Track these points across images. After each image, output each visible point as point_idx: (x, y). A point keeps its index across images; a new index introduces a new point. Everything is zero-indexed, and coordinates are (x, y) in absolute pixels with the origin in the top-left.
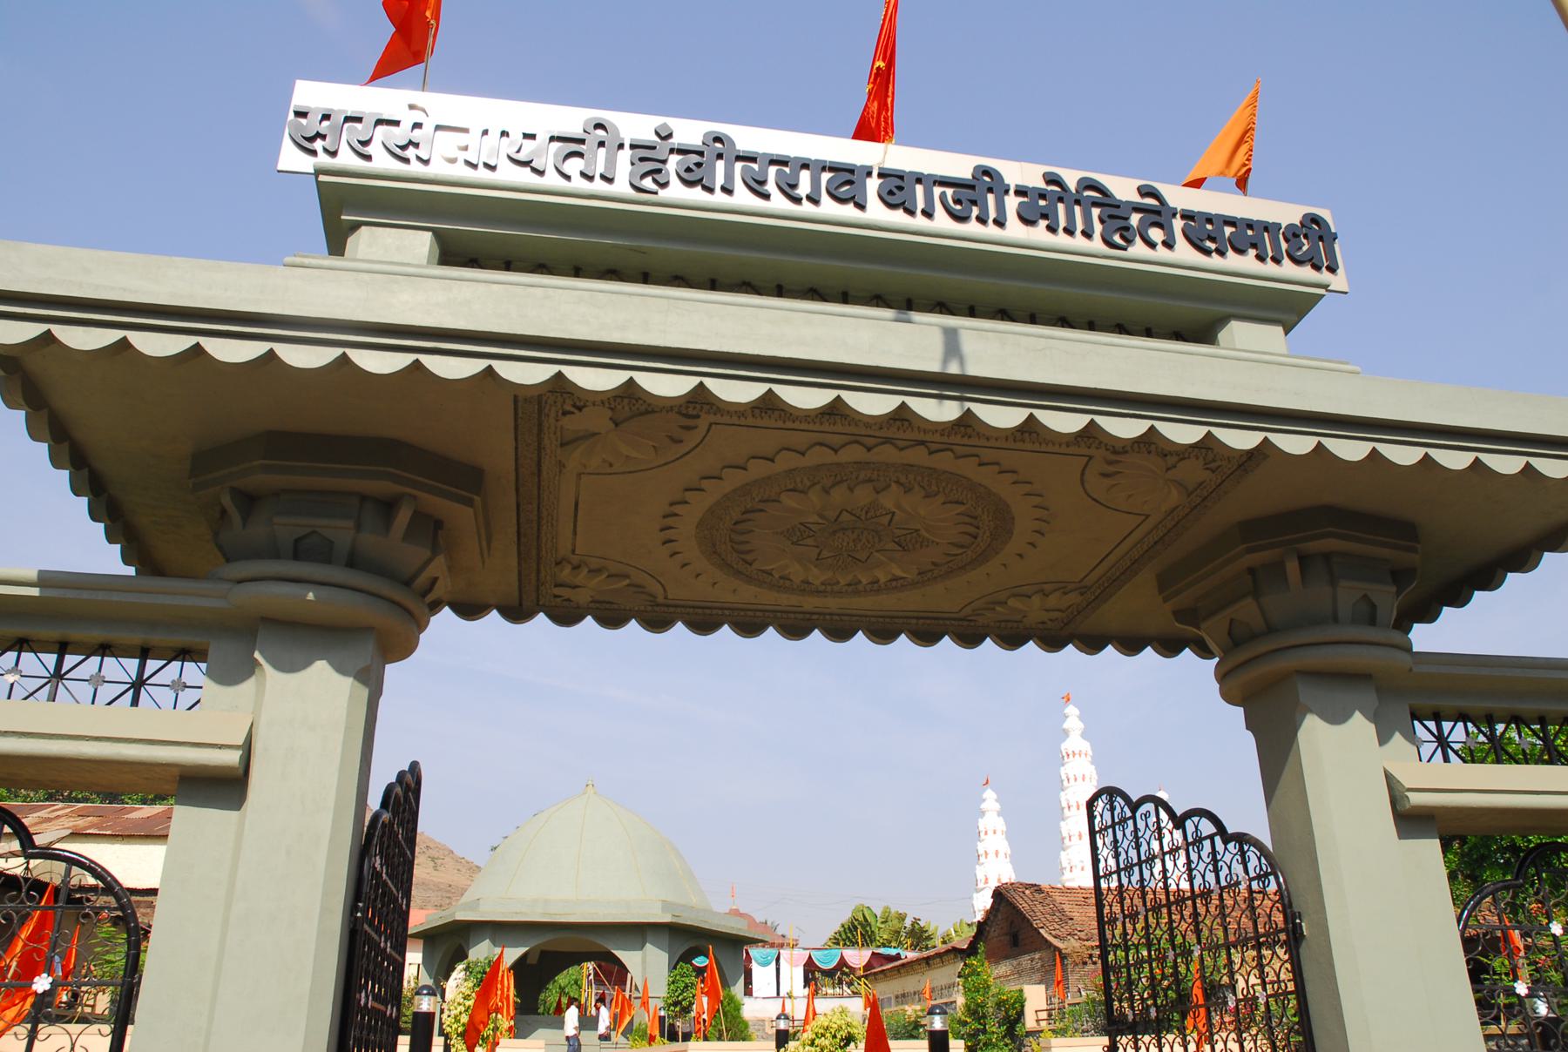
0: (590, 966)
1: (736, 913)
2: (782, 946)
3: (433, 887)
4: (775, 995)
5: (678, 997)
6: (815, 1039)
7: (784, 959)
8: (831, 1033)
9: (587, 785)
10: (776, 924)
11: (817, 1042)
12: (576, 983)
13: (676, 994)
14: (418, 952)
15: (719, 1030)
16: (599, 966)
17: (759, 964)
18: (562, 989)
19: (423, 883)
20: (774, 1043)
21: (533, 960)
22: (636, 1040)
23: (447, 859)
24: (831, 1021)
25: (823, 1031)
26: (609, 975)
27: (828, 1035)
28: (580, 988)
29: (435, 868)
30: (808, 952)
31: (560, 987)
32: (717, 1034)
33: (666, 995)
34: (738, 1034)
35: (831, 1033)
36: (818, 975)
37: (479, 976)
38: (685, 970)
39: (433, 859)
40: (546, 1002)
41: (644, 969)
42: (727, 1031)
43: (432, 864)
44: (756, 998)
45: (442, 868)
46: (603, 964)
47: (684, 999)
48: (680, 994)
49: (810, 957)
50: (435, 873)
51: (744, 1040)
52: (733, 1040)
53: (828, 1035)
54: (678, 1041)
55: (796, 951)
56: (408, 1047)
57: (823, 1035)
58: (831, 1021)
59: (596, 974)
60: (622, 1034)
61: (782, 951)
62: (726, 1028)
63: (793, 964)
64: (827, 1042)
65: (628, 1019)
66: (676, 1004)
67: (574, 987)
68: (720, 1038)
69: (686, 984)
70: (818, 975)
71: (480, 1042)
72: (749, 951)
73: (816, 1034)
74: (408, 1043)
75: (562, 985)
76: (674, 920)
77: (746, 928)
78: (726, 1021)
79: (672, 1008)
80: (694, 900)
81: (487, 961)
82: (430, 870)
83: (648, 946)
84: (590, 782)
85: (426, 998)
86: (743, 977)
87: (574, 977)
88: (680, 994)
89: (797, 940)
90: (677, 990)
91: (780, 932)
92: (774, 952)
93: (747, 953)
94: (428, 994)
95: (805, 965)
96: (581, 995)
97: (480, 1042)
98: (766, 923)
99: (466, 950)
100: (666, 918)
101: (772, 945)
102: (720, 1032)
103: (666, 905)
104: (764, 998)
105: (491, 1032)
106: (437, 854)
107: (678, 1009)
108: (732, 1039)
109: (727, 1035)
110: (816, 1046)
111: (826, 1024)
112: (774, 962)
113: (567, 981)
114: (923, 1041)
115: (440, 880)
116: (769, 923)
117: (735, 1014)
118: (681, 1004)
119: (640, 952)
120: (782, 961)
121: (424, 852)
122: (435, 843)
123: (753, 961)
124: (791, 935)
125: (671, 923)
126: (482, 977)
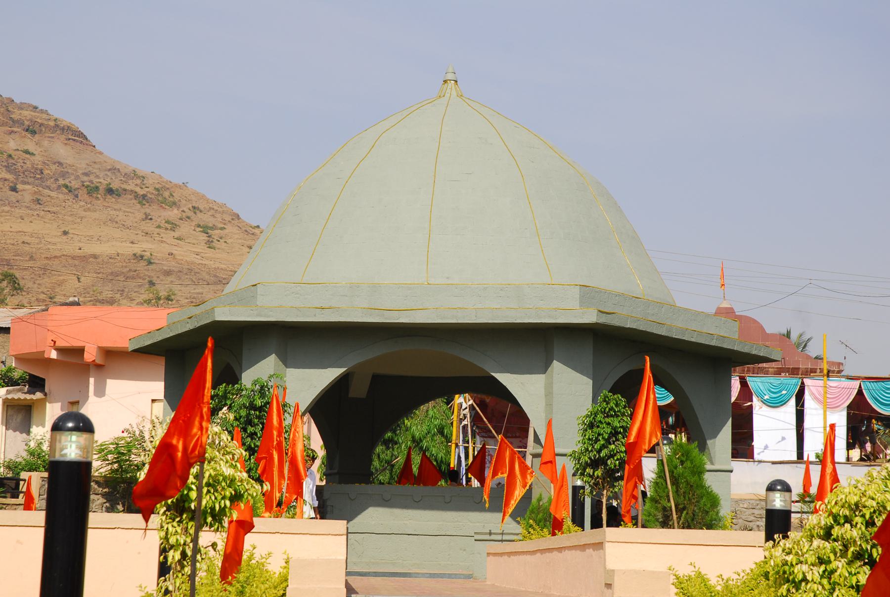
0: (463, 401)
1: (728, 313)
2: (810, 372)
3: (207, 277)
4: (794, 457)
5: (599, 451)
6: (832, 527)
7: (812, 394)
8: (863, 516)
9: (445, 81)
10: (805, 338)
11: (836, 531)
12: (441, 431)
13: (597, 446)
14: (160, 380)
15: (664, 509)
16: (482, 404)
17: (764, 402)
18: (417, 442)
19: (190, 270)
20: (762, 534)
21: (359, 390)
22: (531, 526)
23: (230, 229)
24: (864, 495)
25: (847, 513)
26: (496, 418)
27: (858, 519)
28: (449, 440)
29: (210, 244)
30: (856, 384)
31: (414, 440)
32: (660, 516)
33: (578, 448)
34: (699, 518)
35: (863, 516)
36: (876, 426)
37: (243, 413)
38: (612, 404)
39: (205, 229)
40: (393, 466)
41: (549, 405)
42: (679, 511)
43: (203, 237)
44: (760, 462)
45: (222, 245)
46: (488, 400)
47: (612, 456)
48: (604, 447)
49: (860, 392)
50: (210, 253)
51: (710, 527)
52: (689, 527)
53: (858, 519)
54: (602, 527)
55: (834, 382)
56: (41, 532)
57: (848, 520)
58: (864, 495)
59: (475, 419)
60: (510, 516)
61: (807, 382)
62: (676, 506)
63: (827, 406)
64: (855, 533)
65: (519, 493)
66: (595, 463)
67: (438, 438)
68: (666, 523)
69: (615, 428)
70: (876, 426)
71: (209, 519)
72: (748, 379)
73: (835, 518)
74: (43, 524)
75: (417, 435)
76: (603, 320)
77: (736, 337)
78: (677, 492)
79: (589, 470)
80: (639, 286)
81: (258, 387)
82: (202, 248)
83: (557, 366)
84: (450, 76)
85: (74, 437)
86: (729, 423)
87: (437, 422)
88: (604, 447)
89: (840, 364)
90: (597, 440)
91: (813, 350)
92: (793, 383)
93: (744, 384)
94: (76, 429)
95: (849, 407)
96: (448, 453)
97: (209, 519)
98: (788, 335)
99: (237, 370)
100: (589, 317)
101: (794, 372)
102: (666, 511)
103: (588, 293)
104: (774, 463)
105: (228, 503)
106: (211, 219)
107: (599, 473)
108: (687, 526)
109: (679, 518)
110: (835, 540)
111: (854, 499)
112: (793, 401)
113: (425, 428)
114: (762, 532)
115: (217, 265)
116: (794, 336)
117: (693, 480)
118: (606, 464)
119: (541, 377)
120: (807, 397)
121: (188, 218)
122: (208, 201)
123: (755, 398)
124: (832, 354)
125: (597, 324)
126: (248, 415)
